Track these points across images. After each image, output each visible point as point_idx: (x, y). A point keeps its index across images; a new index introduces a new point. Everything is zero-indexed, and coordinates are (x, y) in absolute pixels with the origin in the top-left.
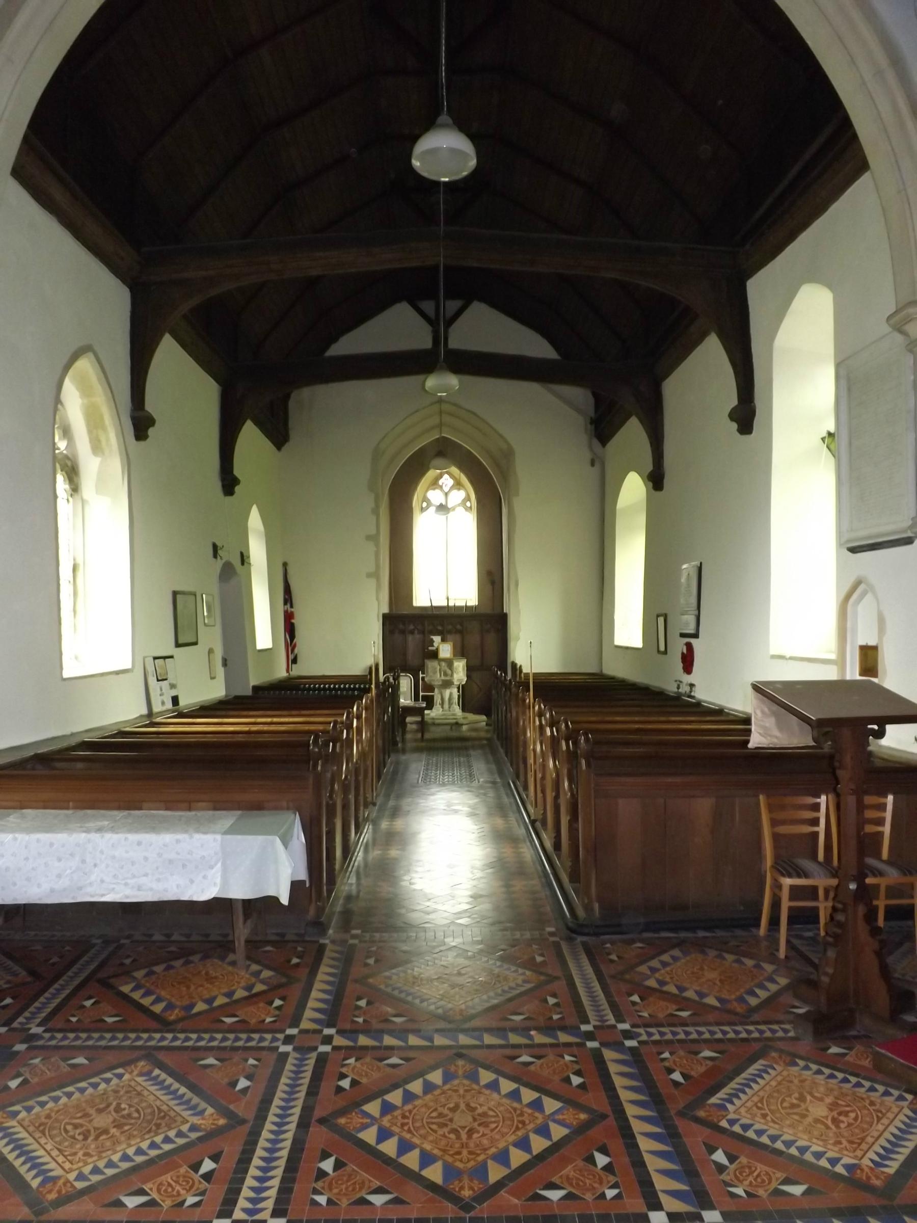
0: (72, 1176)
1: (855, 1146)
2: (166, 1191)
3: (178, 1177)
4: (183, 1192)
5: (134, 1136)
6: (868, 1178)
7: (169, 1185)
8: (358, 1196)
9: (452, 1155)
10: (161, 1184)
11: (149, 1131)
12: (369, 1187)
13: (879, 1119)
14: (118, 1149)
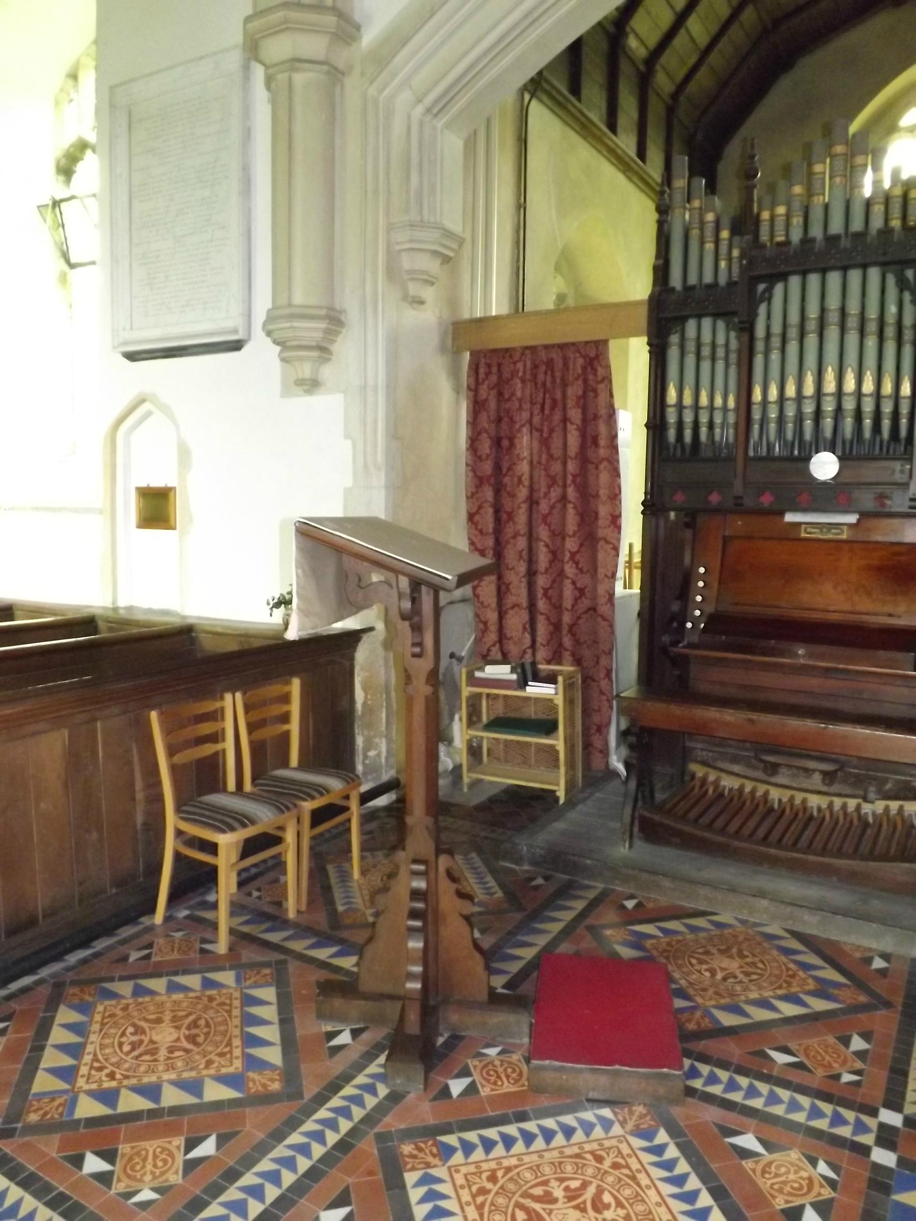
0: (617, 1130)
1: (107, 1014)
2: (514, 1071)
3: (495, 1083)
4: (497, 1063)
5: (764, 988)
7: (508, 1077)
8: (775, 1156)
9: (628, 1166)
10: (516, 1081)
11: (508, 1170)
12: (757, 1162)
13: (95, 1059)
14: (555, 1153)
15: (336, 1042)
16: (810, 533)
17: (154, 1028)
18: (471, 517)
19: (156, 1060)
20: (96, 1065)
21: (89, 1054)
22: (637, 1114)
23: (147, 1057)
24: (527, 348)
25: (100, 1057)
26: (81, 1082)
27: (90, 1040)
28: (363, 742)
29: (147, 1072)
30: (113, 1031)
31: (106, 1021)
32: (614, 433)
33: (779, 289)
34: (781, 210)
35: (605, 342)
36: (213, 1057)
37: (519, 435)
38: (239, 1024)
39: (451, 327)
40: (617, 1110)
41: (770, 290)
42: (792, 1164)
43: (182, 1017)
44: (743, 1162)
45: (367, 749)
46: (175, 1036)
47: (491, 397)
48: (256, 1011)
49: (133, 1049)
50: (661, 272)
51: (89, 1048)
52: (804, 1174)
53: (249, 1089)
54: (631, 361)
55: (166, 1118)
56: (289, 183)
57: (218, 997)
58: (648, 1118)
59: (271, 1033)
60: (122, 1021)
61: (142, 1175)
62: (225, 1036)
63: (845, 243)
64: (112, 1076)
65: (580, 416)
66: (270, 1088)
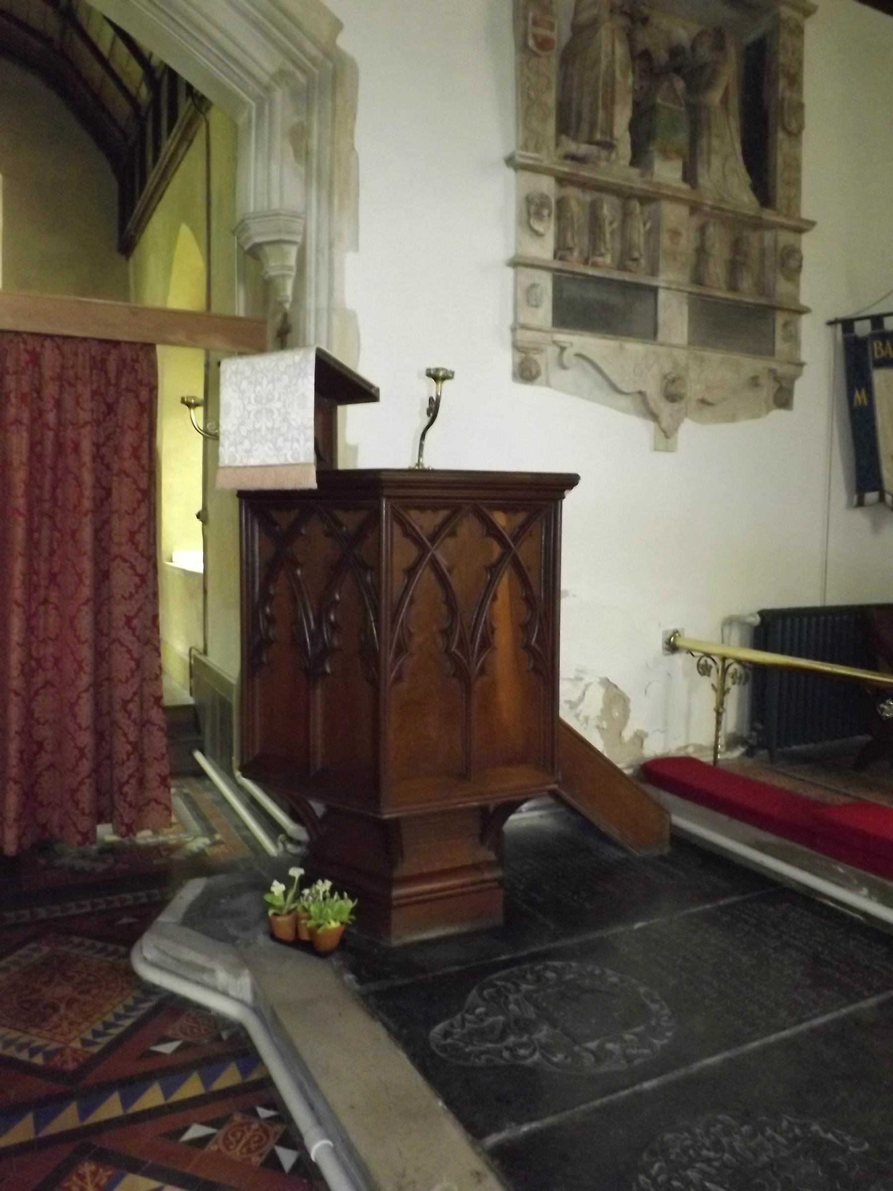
22: (88, 1175)
42: (242, 1125)
44: (206, 1150)
52: (255, 1126)
56: (827, 555)
58: (101, 1171)
61: (257, 1130)
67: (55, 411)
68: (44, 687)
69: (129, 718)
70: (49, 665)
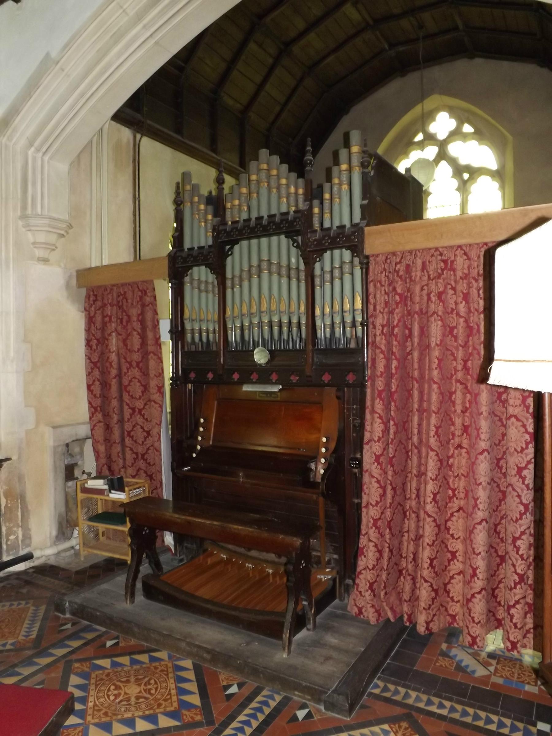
1: (98, 679)
6: (82, 665)
15: (230, 691)
16: (261, 397)
17: (126, 686)
18: (89, 387)
19: (129, 704)
20: (96, 708)
21: (91, 702)
22: (403, 728)
23: (125, 703)
24: (114, 285)
25: (97, 703)
26: (89, 718)
27: (90, 694)
28: (6, 531)
29: (126, 711)
30: (103, 688)
31: (98, 683)
32: (158, 336)
33: (237, 248)
34: (237, 202)
35: (151, 282)
36: (161, 702)
37: (110, 338)
38: (173, 682)
39: (75, 274)
40: (392, 726)
41: (232, 248)
43: (141, 679)
45: (8, 535)
46: (138, 690)
47: (97, 315)
48: (183, 674)
49: (116, 698)
50: (178, 239)
51: (91, 699)
53: (184, 720)
54: (165, 292)
55: (173, 733)
57: (159, 667)
59: (193, 687)
60: (107, 682)
62: (167, 689)
63: (265, 222)
64: (106, 714)
65: (139, 326)
66: (196, 719)
67: (464, 302)
68: (458, 511)
69: (523, 483)
70: (462, 495)
